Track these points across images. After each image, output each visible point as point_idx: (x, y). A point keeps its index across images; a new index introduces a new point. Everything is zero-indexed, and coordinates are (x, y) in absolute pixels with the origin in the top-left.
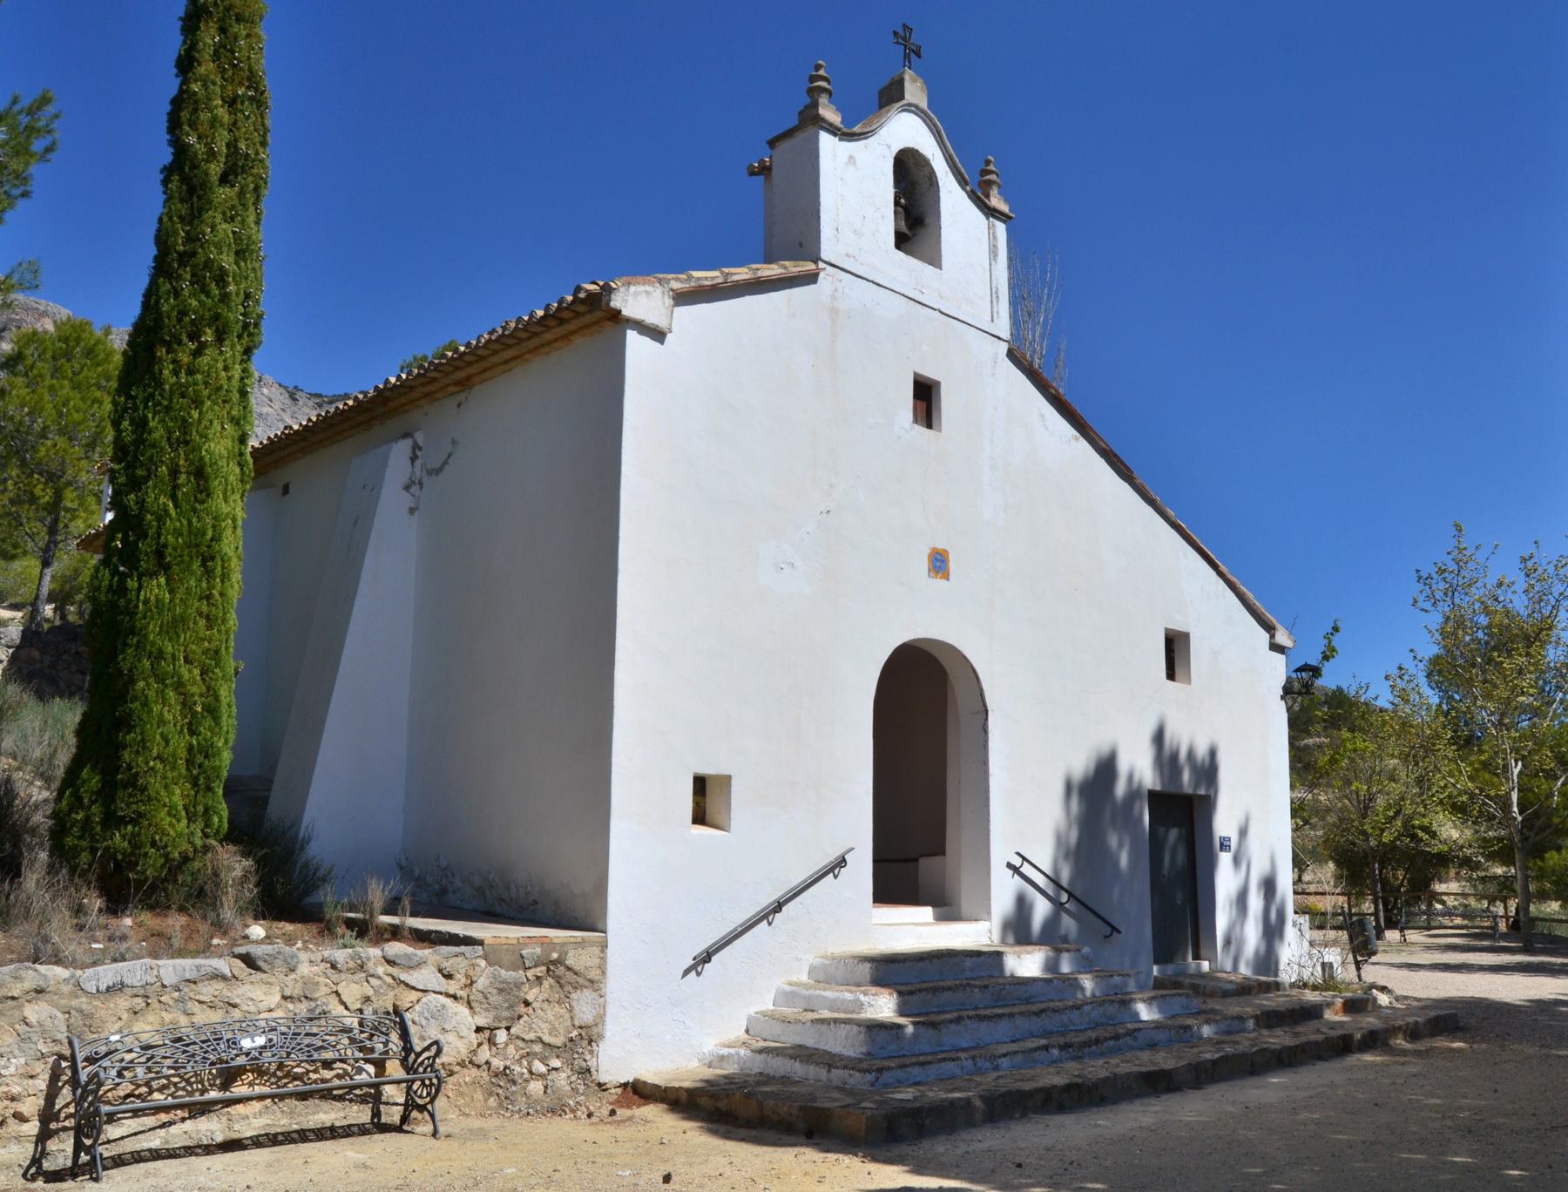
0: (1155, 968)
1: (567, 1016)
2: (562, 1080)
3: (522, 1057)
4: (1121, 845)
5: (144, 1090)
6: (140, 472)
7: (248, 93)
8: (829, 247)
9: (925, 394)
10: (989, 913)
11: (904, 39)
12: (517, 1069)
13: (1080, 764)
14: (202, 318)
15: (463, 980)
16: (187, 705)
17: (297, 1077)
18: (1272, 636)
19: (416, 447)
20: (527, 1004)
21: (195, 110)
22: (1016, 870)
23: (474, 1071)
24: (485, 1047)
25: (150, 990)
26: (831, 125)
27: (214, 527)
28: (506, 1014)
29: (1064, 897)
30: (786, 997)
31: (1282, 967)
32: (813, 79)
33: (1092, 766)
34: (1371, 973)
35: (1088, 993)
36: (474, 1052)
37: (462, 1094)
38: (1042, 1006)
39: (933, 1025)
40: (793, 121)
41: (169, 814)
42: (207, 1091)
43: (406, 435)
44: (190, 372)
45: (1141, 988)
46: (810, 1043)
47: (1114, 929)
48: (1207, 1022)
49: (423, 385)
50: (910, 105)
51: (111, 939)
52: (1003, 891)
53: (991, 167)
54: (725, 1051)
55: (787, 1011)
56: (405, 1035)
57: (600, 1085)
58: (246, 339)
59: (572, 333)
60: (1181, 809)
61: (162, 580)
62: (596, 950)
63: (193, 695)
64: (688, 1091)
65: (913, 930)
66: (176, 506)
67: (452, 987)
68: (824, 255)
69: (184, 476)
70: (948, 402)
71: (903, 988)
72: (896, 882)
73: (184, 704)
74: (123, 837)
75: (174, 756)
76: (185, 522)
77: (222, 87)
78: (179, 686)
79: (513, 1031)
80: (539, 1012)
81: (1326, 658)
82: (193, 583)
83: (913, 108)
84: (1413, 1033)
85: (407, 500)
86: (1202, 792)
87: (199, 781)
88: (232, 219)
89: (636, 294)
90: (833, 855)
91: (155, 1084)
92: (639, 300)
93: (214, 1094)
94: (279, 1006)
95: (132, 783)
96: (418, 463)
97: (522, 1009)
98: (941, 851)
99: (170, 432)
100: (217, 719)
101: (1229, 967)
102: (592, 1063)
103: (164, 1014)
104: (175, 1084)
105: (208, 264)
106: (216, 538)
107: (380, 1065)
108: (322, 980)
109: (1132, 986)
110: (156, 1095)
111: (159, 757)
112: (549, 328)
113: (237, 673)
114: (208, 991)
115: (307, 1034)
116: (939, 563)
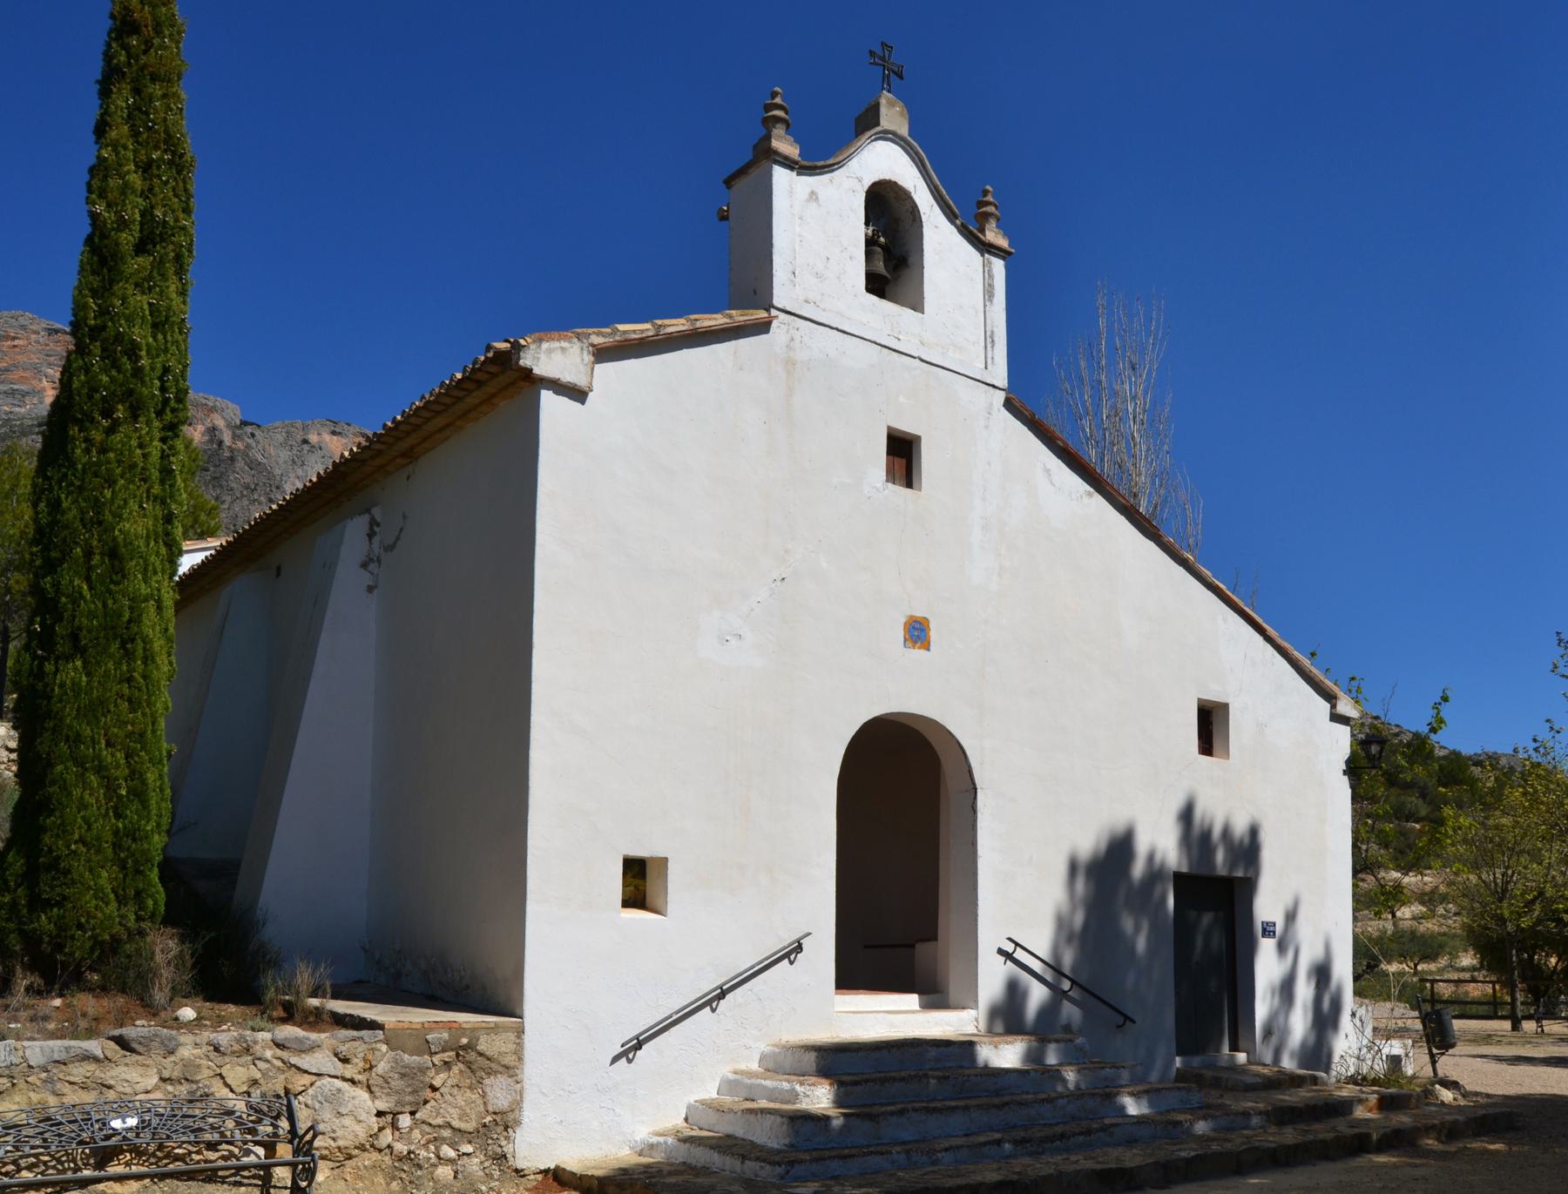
0: (1178, 1059)
1: (480, 1102)
2: (474, 1165)
3: (429, 1142)
4: (1137, 929)
5: (11, 1168)
6: (54, 554)
7: (167, 159)
8: (780, 297)
9: (903, 453)
10: (976, 1001)
11: (883, 59)
12: (423, 1153)
13: (1088, 841)
14: (114, 394)
15: (361, 1064)
16: (110, 786)
17: (178, 1158)
18: (1333, 706)
19: (373, 523)
20: (434, 1089)
21: (106, 177)
22: (1008, 956)
23: (375, 1156)
24: (388, 1131)
25: (16, 1071)
26: (786, 158)
27: (131, 608)
28: (409, 1098)
29: (1066, 985)
30: (729, 1086)
31: (1336, 1058)
32: (768, 108)
33: (1103, 846)
34: (1449, 1065)
35: (1071, 1086)
36: (375, 1136)
37: (361, 1178)
38: (1007, 1099)
39: (871, 1117)
40: (748, 156)
41: (96, 897)
42: (80, 1170)
43: (368, 511)
44: (103, 450)
45: (1135, 1081)
46: (740, 1133)
47: (1127, 1018)
48: (1205, 1118)
49: (372, 458)
50: (886, 132)
51: (32, 1019)
52: (991, 978)
53: (990, 198)
54: (655, 1140)
55: (727, 1099)
56: (291, 1118)
57: (517, 1171)
58: (168, 416)
59: (493, 396)
60: (1214, 892)
61: (79, 663)
62: (512, 1036)
63: (117, 779)
64: (599, 1179)
65: (889, 1016)
66: (91, 588)
67: (349, 1071)
68: (776, 302)
69: (97, 557)
70: (929, 459)
71: (845, 1078)
72: (860, 967)
73: (108, 788)
74: (49, 919)
75: (98, 839)
76: (100, 605)
77: (135, 151)
78: (100, 770)
79: (418, 1116)
80: (448, 1097)
81: (1434, 730)
82: (111, 665)
83: (895, 138)
84: (1451, 1132)
85: (365, 578)
86: (1240, 874)
87: (131, 867)
88: (150, 289)
89: (550, 351)
90: (787, 938)
91: (23, 1163)
92: (553, 357)
93: (87, 1173)
94: (156, 1088)
95: (54, 865)
96: (376, 540)
97: (428, 1093)
98: (934, 937)
99: (82, 512)
100: (145, 804)
101: (1268, 1059)
102: (508, 1149)
103: (32, 1094)
104: (45, 1163)
105: (119, 338)
106: (136, 619)
107: (270, 1148)
108: (204, 1062)
109: (1125, 1076)
110: (25, 1174)
111: (82, 841)
112: (470, 391)
113: (169, 755)
114: (79, 1072)
115: (184, 1116)
116: (917, 633)
